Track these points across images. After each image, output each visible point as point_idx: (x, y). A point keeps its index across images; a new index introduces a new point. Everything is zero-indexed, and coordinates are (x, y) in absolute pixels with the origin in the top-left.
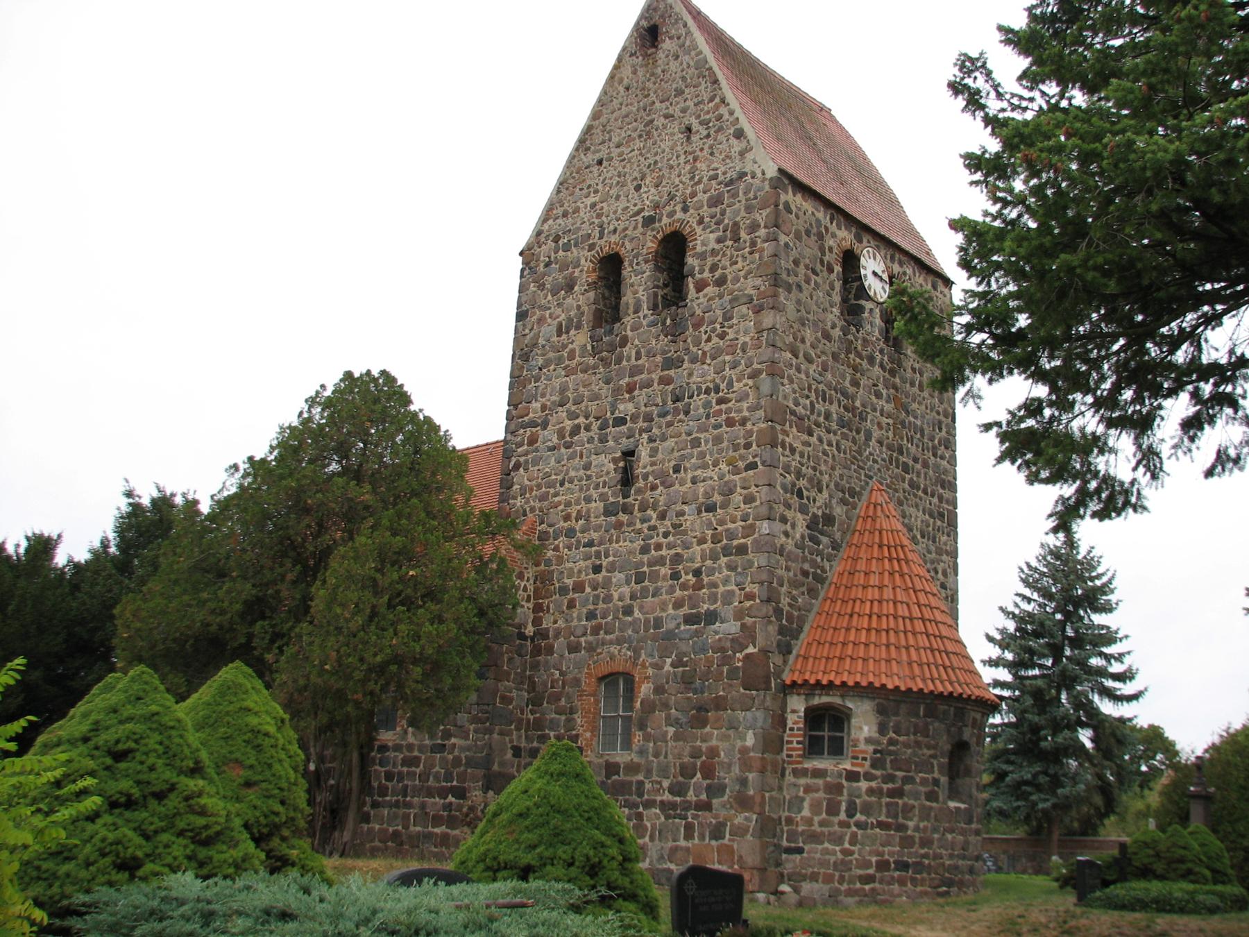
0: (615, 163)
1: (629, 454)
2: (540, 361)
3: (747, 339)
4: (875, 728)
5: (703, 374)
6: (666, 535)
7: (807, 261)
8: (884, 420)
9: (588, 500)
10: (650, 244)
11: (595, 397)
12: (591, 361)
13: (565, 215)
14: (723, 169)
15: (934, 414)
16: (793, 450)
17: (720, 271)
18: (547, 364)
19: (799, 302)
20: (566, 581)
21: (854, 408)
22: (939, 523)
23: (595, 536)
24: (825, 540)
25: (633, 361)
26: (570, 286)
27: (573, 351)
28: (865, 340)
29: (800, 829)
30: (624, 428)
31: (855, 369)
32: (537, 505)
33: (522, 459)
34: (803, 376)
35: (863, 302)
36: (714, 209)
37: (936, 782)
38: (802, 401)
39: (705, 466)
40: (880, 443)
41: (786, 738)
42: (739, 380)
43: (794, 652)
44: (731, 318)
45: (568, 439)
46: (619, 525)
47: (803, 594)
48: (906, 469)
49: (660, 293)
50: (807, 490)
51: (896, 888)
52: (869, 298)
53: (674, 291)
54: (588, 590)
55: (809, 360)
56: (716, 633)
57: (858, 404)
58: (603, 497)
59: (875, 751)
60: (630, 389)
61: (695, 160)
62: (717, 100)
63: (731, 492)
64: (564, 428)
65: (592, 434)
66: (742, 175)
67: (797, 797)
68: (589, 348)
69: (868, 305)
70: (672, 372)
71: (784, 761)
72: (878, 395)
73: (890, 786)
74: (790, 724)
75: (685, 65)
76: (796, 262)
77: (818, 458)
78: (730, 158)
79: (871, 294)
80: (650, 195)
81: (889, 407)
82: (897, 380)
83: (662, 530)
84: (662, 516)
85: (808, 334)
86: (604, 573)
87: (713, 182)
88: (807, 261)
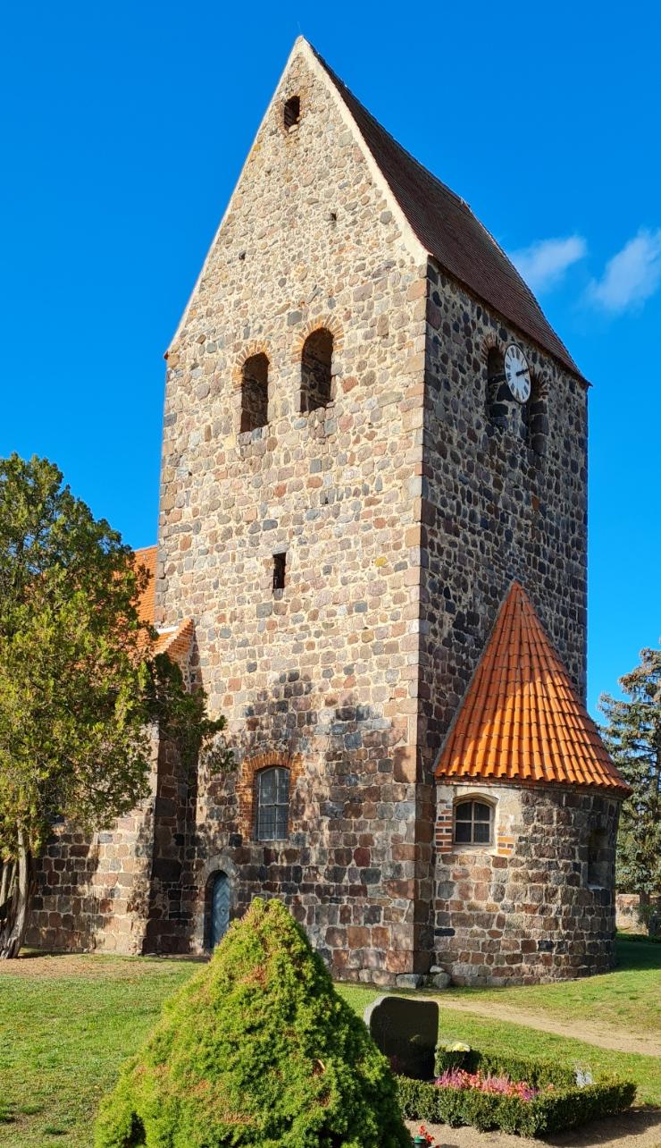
0: (259, 256)
1: (280, 560)
2: (190, 466)
3: (396, 439)
4: (520, 817)
5: (351, 476)
6: (318, 634)
7: (455, 357)
8: (524, 522)
9: (241, 601)
10: (296, 343)
11: (246, 501)
12: (241, 466)
13: (209, 313)
14: (370, 258)
15: (568, 515)
16: (441, 551)
17: (368, 369)
18: (198, 467)
19: (446, 401)
20: (222, 679)
21: (497, 509)
22: (570, 621)
23: (248, 635)
24: (469, 638)
25: (283, 465)
26: (217, 389)
27: (222, 455)
28: (507, 441)
29: (450, 912)
30: (274, 531)
31: (499, 470)
32: (192, 607)
33: (176, 563)
34: (450, 477)
35: (505, 402)
36: (361, 303)
37: (576, 867)
38: (449, 501)
39: (355, 567)
40: (520, 542)
41: (436, 827)
42: (388, 480)
43: (443, 745)
44: (379, 419)
45: (220, 542)
46: (272, 626)
47: (450, 690)
48: (542, 568)
49: (308, 394)
50: (454, 589)
51: (540, 968)
52: (511, 398)
53: (321, 392)
54: (244, 688)
55: (456, 460)
56: (368, 728)
57: (500, 505)
58: (255, 599)
59: (521, 839)
60: (280, 491)
61: (341, 250)
62: (363, 181)
63: (381, 592)
64: (216, 532)
65: (243, 537)
66: (390, 265)
67: (447, 882)
68: (238, 451)
69: (511, 406)
70: (320, 475)
71: (434, 848)
72: (519, 497)
73: (535, 871)
74: (439, 814)
75: (329, 143)
76: (445, 359)
77: (464, 559)
78: (377, 245)
79: (514, 394)
80: (296, 291)
81: (529, 509)
82: (536, 482)
83: (313, 630)
84: (314, 617)
85: (455, 433)
86: (258, 671)
87: (360, 273)
88: (455, 357)
